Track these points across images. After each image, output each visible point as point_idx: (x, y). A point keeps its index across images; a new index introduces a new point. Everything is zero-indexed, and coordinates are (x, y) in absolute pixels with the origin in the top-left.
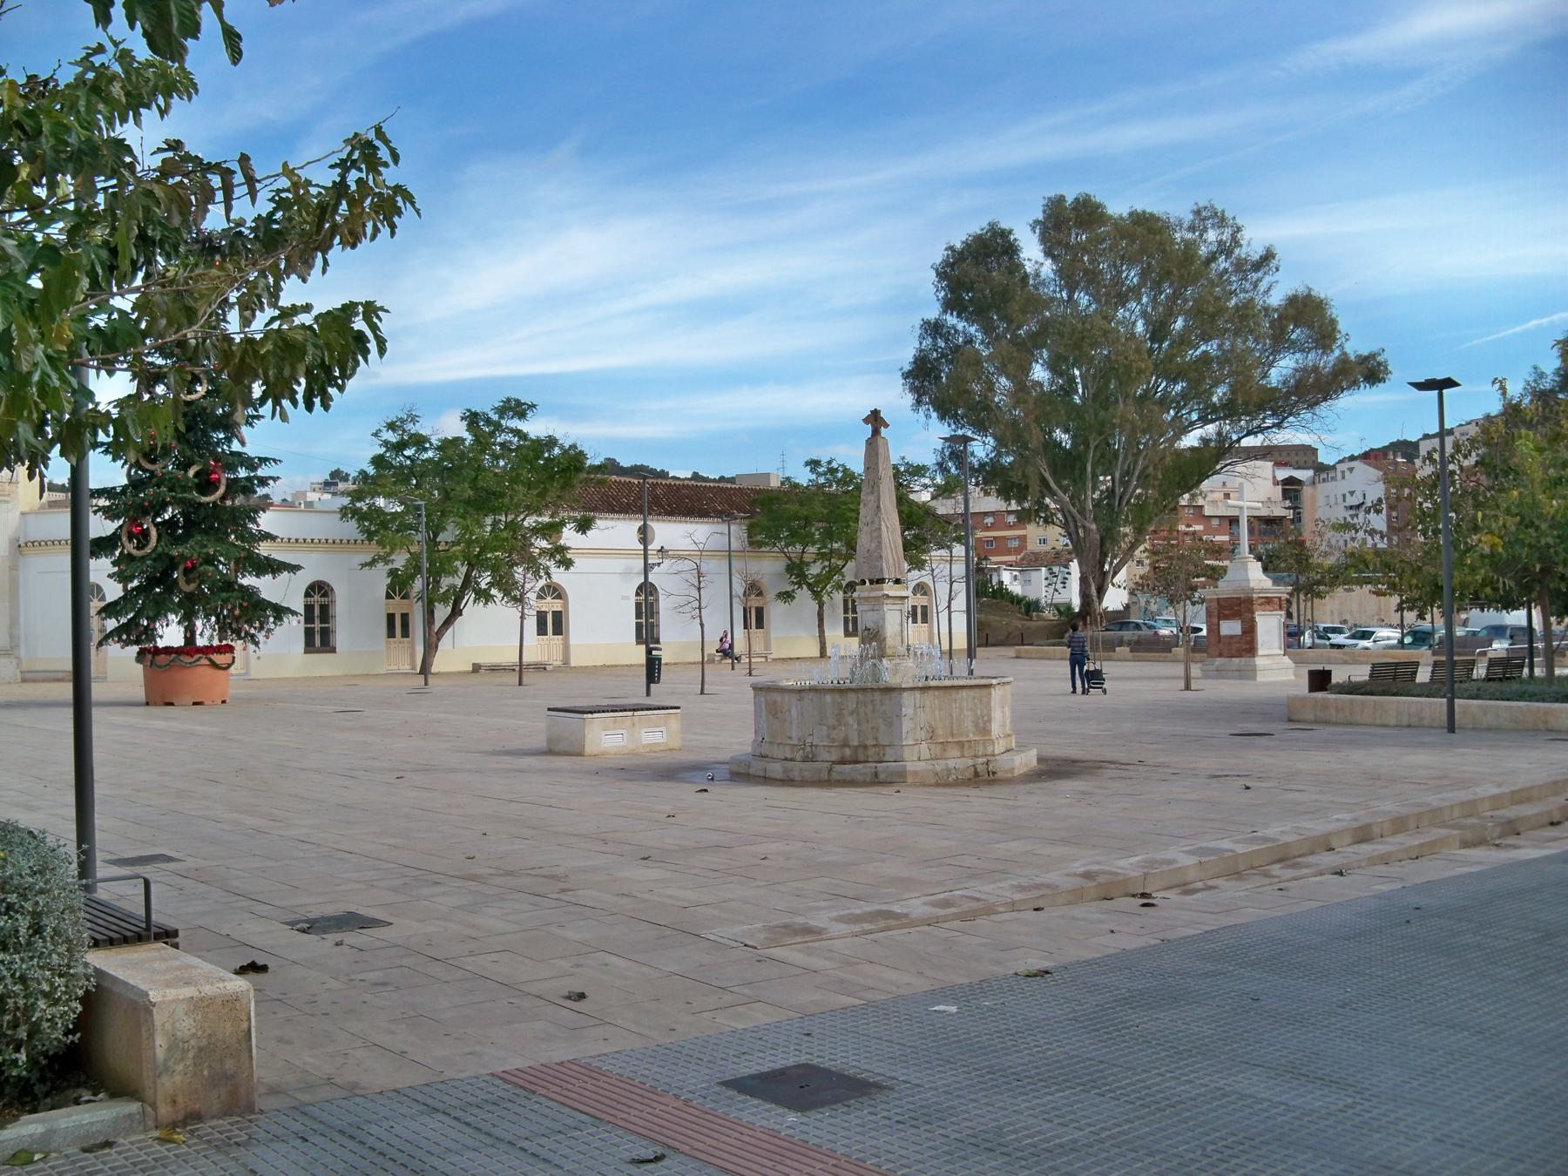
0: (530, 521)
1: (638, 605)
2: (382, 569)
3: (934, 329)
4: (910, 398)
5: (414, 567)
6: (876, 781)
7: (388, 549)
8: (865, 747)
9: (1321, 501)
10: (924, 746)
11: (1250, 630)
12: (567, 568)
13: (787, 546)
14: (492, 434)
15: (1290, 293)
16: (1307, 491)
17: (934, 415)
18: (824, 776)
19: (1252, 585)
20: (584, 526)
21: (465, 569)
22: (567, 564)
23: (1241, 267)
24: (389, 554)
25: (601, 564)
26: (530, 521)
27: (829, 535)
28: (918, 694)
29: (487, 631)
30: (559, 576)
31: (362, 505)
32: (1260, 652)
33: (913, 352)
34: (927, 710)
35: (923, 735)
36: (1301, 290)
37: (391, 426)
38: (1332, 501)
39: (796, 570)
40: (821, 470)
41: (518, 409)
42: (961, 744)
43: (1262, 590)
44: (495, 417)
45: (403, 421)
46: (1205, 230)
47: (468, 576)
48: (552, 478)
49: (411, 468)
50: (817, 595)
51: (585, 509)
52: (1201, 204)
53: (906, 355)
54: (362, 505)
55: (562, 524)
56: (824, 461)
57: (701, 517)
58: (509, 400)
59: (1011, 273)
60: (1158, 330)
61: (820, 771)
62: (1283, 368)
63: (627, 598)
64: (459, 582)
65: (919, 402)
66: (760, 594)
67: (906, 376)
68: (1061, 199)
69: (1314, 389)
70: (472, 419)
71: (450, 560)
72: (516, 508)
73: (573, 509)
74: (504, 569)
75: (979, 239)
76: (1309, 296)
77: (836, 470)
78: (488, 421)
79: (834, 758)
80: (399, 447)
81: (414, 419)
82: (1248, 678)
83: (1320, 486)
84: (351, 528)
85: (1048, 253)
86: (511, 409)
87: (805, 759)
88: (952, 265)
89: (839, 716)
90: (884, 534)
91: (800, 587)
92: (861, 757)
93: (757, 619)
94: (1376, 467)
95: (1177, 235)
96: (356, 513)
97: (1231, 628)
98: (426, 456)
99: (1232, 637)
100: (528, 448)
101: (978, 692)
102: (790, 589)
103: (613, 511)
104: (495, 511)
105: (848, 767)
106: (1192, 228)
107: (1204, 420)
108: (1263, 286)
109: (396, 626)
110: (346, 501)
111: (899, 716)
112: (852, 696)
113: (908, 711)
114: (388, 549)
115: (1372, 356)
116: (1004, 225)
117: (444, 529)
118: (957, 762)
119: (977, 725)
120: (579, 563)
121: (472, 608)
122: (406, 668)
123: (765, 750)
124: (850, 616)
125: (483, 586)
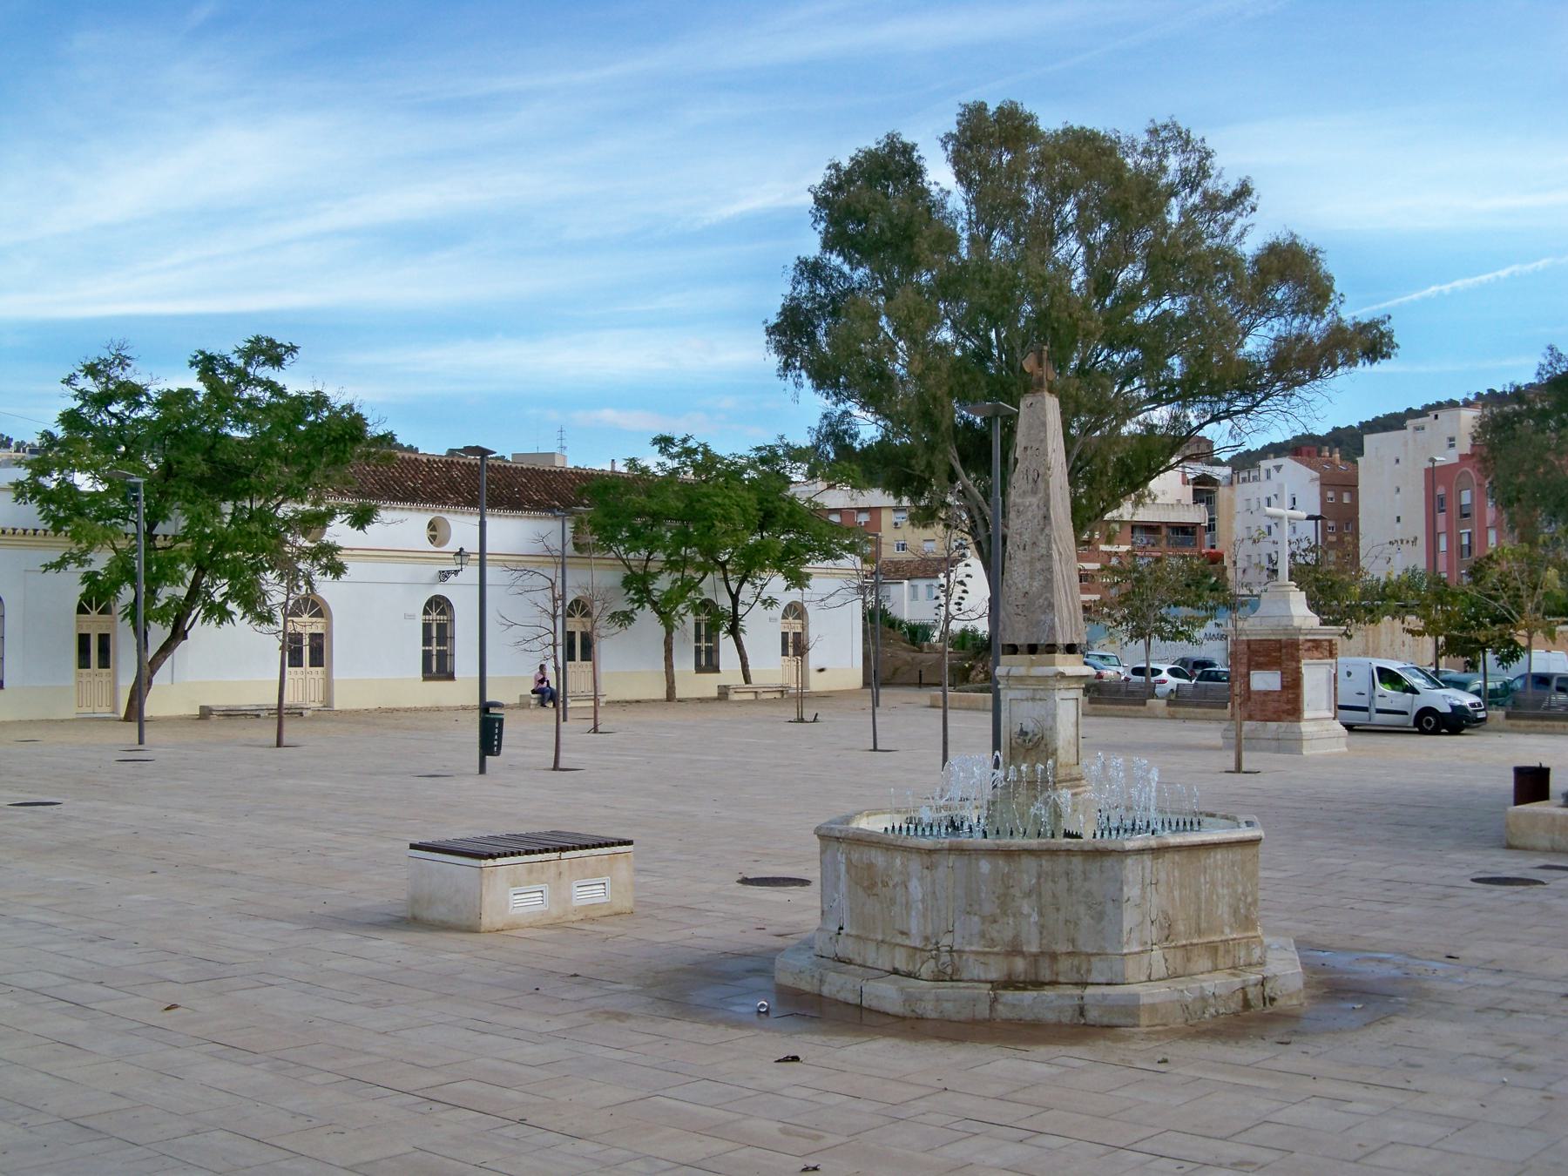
0: (286, 510)
1: (427, 628)
2: (74, 573)
3: (812, 270)
4: (775, 360)
5: (124, 571)
6: (1082, 1028)
7: (84, 545)
8: (1054, 957)
9: (1239, 506)
10: (1157, 953)
11: (1293, 685)
12: (337, 575)
13: (627, 552)
14: (236, 385)
15: (1270, 241)
16: (1222, 493)
17: (807, 383)
18: (983, 1011)
19: (1297, 623)
20: (361, 519)
21: (191, 574)
22: (337, 570)
23: (1214, 204)
24: (85, 552)
25: (381, 567)
26: (286, 510)
27: (684, 539)
28: (1147, 859)
29: (227, 660)
30: (326, 587)
31: (50, 483)
32: (1307, 715)
33: (781, 301)
34: (1162, 889)
35: (1153, 933)
36: (1284, 238)
37: (92, 371)
38: (1254, 506)
39: (638, 584)
40: (674, 450)
41: (272, 353)
42: (1212, 949)
43: (1311, 631)
44: (240, 363)
45: (108, 364)
46: (1165, 154)
47: (196, 583)
48: (319, 451)
49: (117, 430)
50: (665, 618)
51: (359, 493)
52: (1159, 122)
53: (773, 300)
54: (50, 483)
55: (331, 514)
56: (678, 437)
57: (512, 508)
58: (258, 340)
59: (914, 201)
60: (1101, 282)
61: (975, 1001)
62: (1257, 342)
63: (412, 617)
64: (182, 592)
65: (787, 366)
66: (588, 614)
67: (771, 331)
68: (981, 108)
69: (1298, 364)
70: (207, 365)
71: (173, 562)
72: (269, 491)
73: (341, 494)
74: (249, 575)
75: (871, 156)
76: (1293, 244)
77: (695, 451)
78: (229, 368)
79: (994, 976)
80: (102, 400)
81: (123, 362)
82: (1291, 751)
83: (1238, 487)
84: (30, 515)
85: (961, 176)
86: (262, 352)
87: (938, 977)
88: (837, 189)
89: (1004, 900)
90: (1056, 567)
91: (641, 605)
92: (1046, 975)
93: (580, 647)
94: (1309, 465)
95: (1129, 160)
96: (46, 497)
97: (1265, 681)
98: (141, 414)
99: (1267, 693)
100: (285, 407)
101: (1236, 855)
102: (628, 608)
103: (395, 498)
104: (236, 495)
105: (1029, 996)
106: (1147, 152)
107: (1157, 400)
108: (1234, 231)
109: (93, 652)
110: (23, 474)
111: (1117, 902)
112: (1029, 864)
113: (1132, 892)
114: (84, 545)
115: (1373, 325)
116: (907, 138)
117: (166, 518)
118: (1216, 983)
119: (1236, 911)
120: (354, 569)
121: (201, 632)
122: (104, 711)
123: (846, 948)
124: (703, 644)
125: (218, 599)
